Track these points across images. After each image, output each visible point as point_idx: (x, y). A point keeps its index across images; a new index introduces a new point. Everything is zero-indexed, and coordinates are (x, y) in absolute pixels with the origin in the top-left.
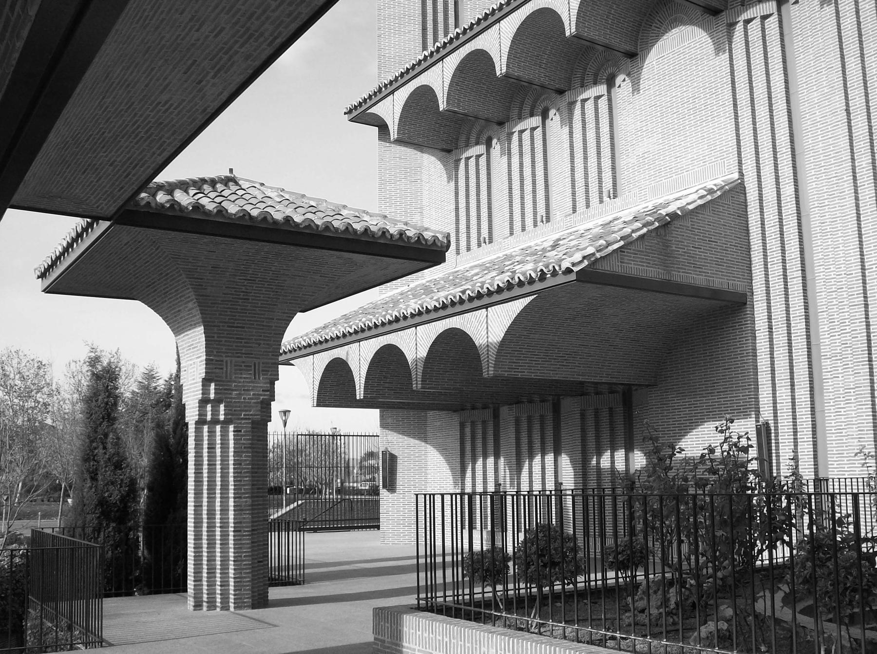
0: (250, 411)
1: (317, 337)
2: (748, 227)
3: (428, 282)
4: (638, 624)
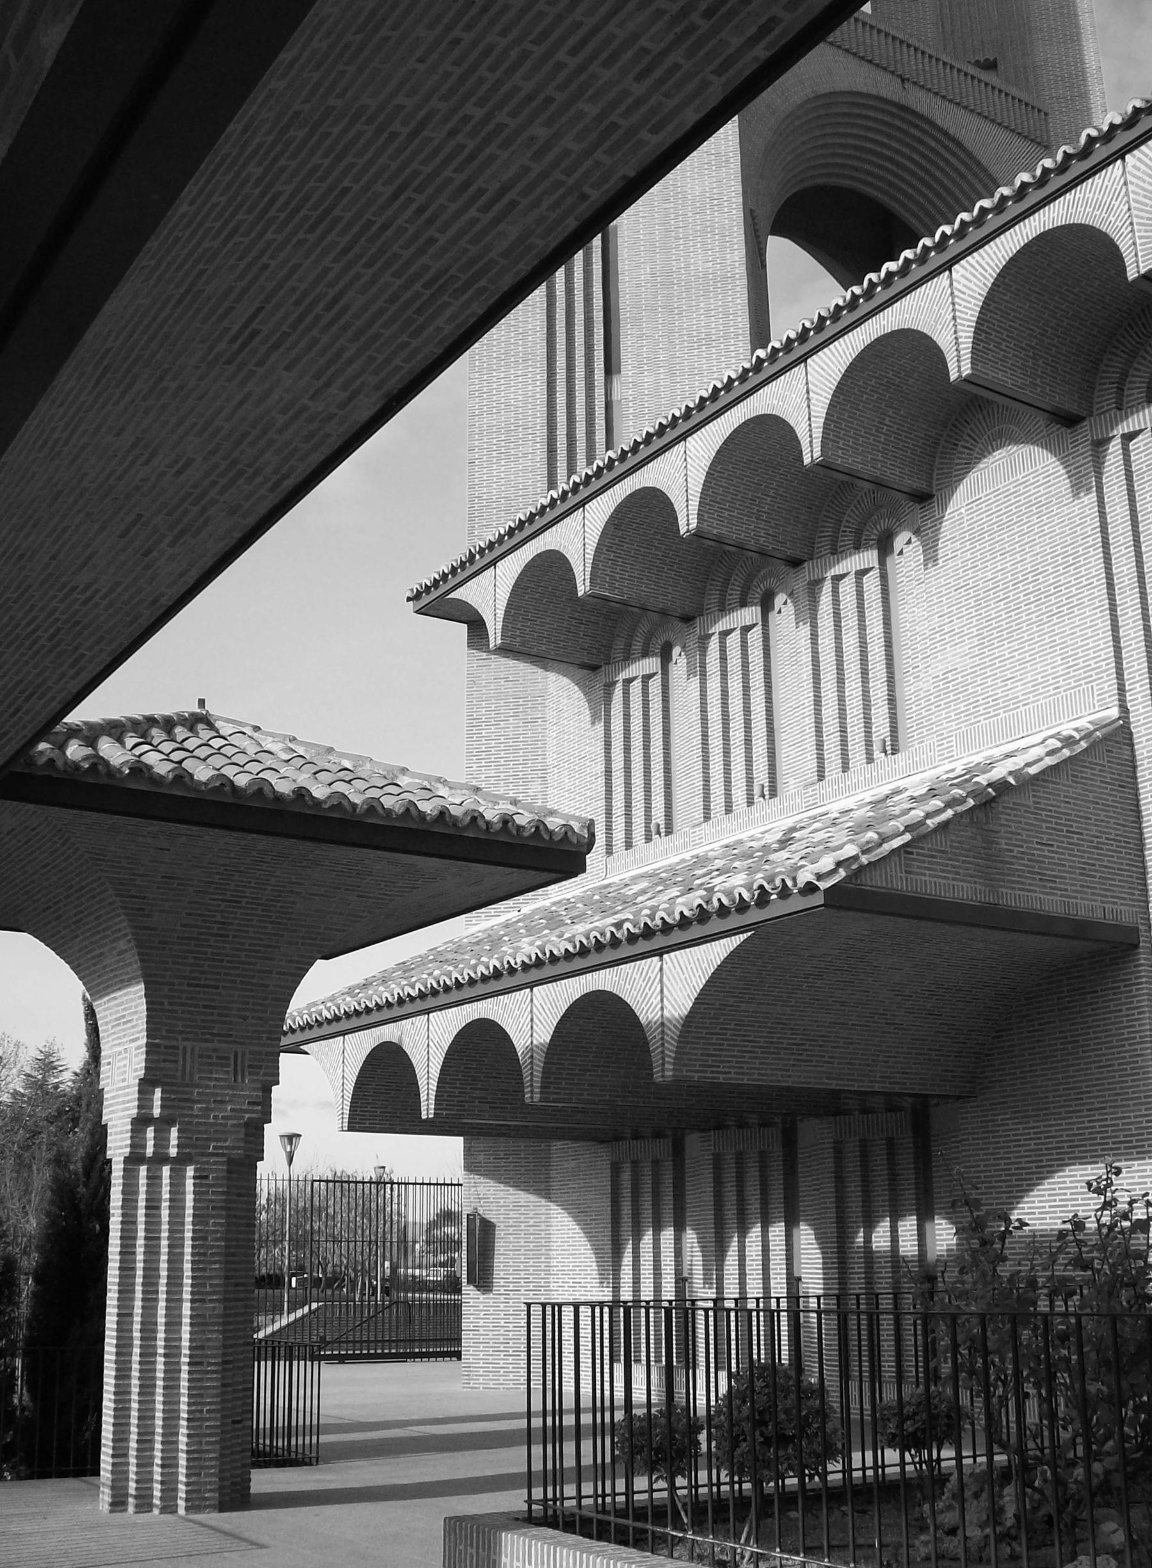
0: (226, 1140)
1: (350, 1004)
2: (1138, 806)
3: (554, 904)
4: (943, 1557)
